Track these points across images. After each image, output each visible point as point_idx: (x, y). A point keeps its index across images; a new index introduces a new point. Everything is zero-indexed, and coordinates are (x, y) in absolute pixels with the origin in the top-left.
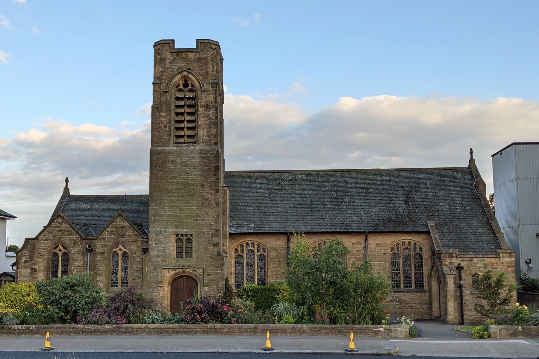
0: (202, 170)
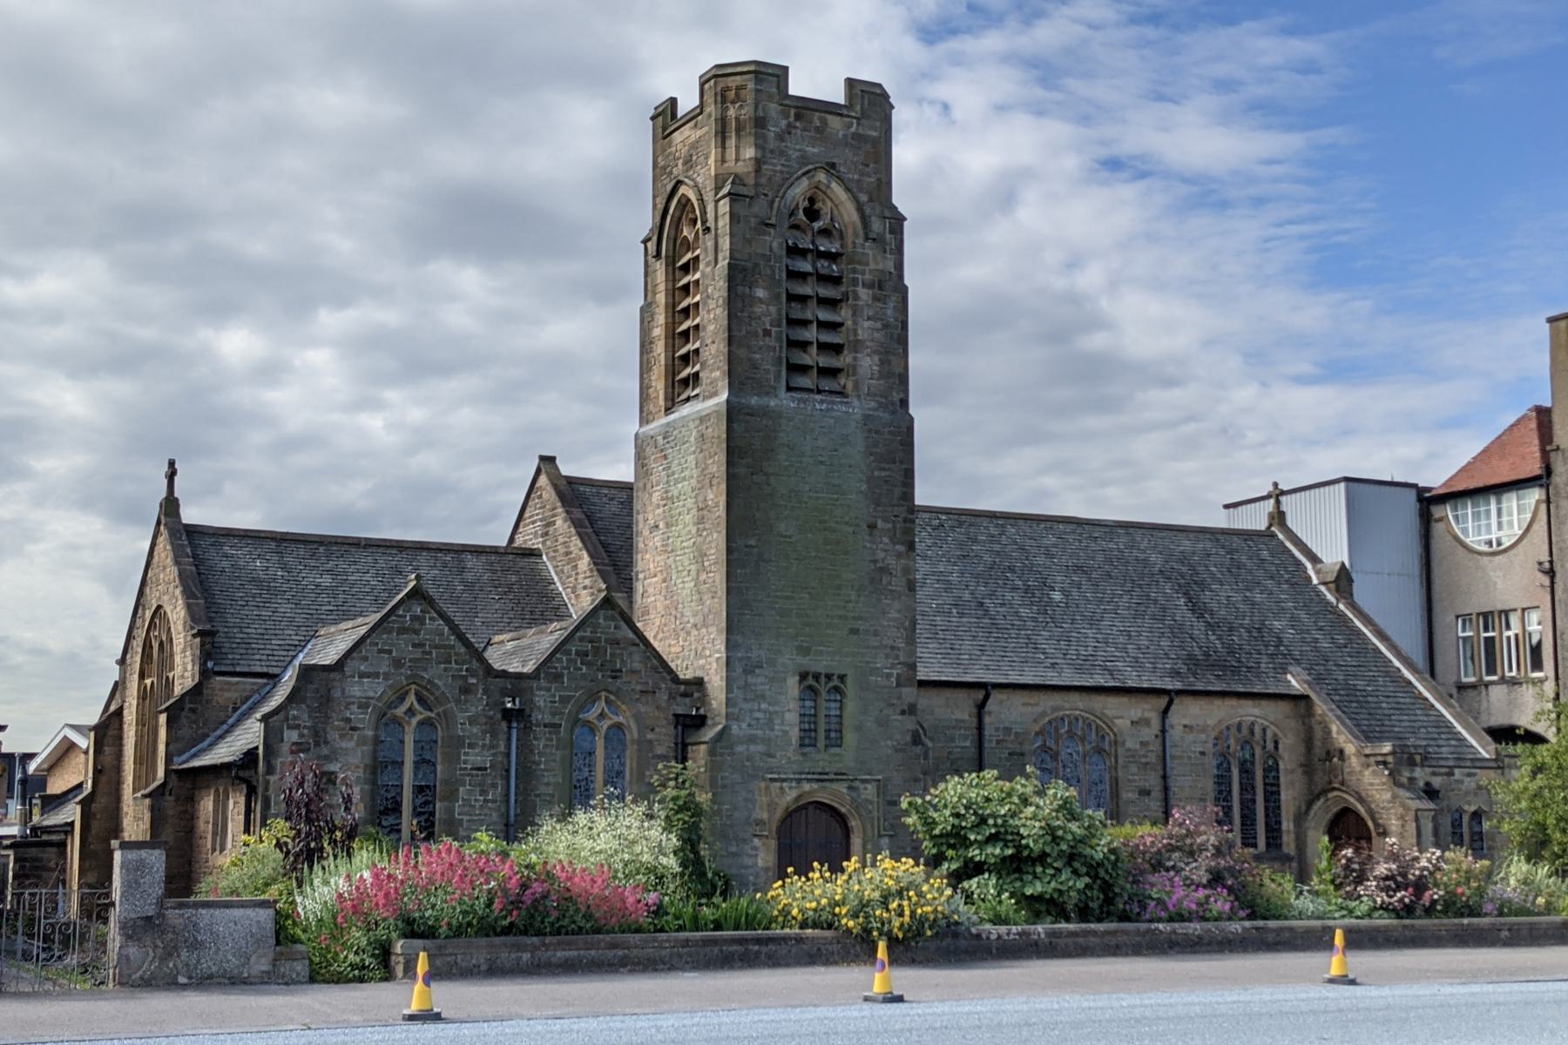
0: (870, 480)
